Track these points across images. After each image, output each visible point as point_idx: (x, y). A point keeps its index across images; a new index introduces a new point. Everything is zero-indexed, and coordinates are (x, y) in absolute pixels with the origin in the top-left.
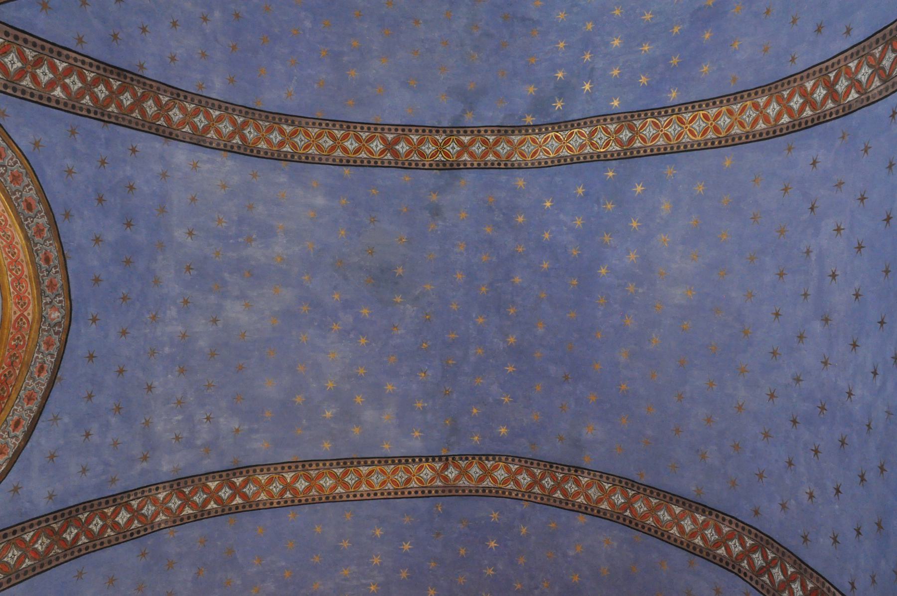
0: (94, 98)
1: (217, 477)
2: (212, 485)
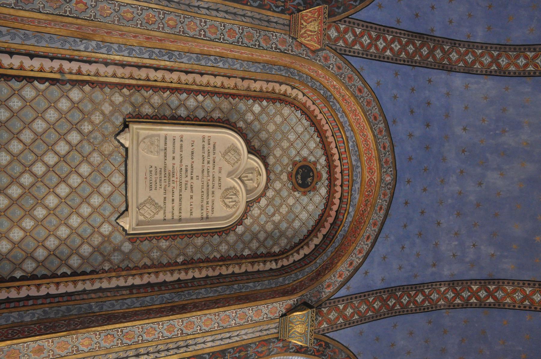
0: (407, 53)
2: (475, 288)
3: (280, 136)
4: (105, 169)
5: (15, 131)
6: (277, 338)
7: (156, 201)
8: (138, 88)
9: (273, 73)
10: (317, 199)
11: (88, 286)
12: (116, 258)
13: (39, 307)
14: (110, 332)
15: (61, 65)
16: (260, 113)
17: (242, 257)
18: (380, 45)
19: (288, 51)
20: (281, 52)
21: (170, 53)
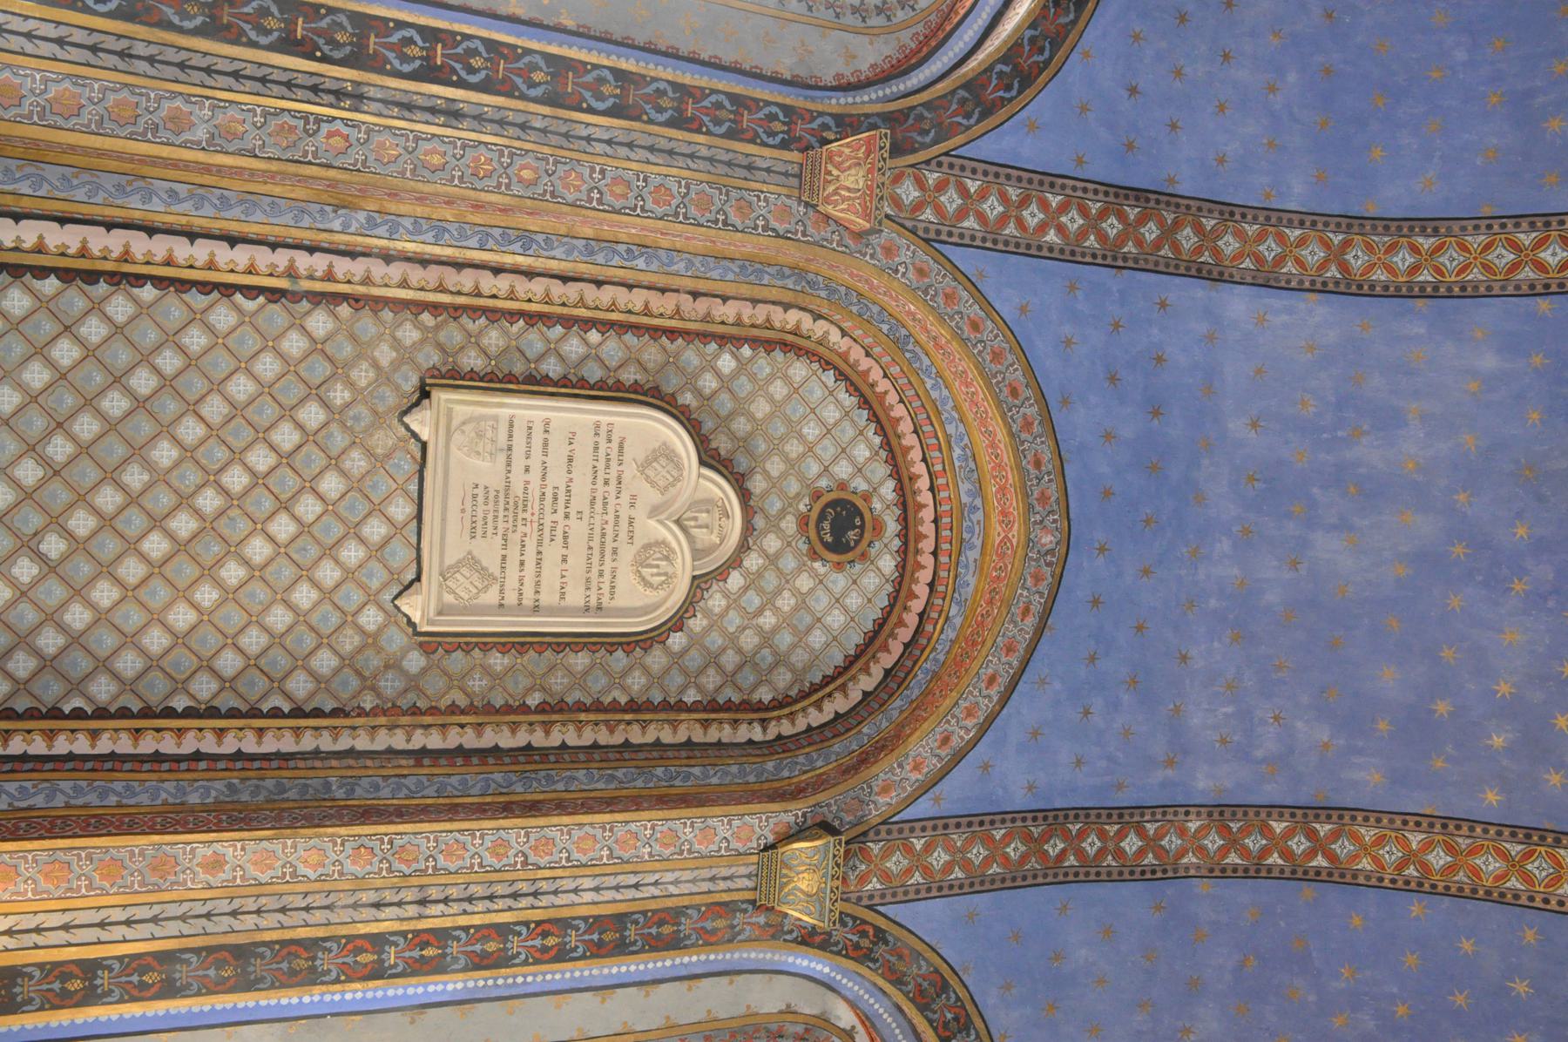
1: (1287, 816)
2: (1278, 827)
3: (782, 430)
4: (374, 487)
5: (192, 398)
6: (753, 902)
7: (485, 564)
8: (456, 311)
9: (765, 282)
10: (871, 581)
11: (326, 743)
12: (390, 685)
13: (221, 774)
14: (366, 841)
15: (292, 261)
16: (735, 375)
17: (680, 707)
18: (1029, 219)
19: (796, 233)
20: (778, 236)
21: (526, 239)
